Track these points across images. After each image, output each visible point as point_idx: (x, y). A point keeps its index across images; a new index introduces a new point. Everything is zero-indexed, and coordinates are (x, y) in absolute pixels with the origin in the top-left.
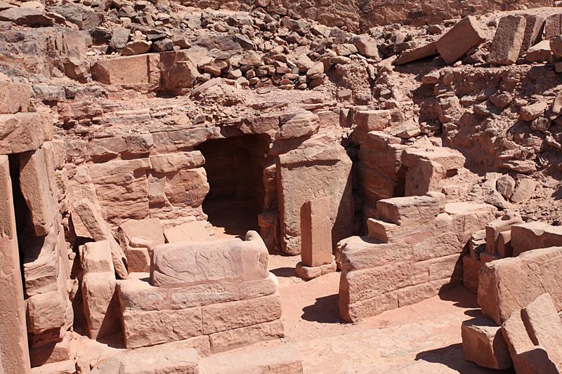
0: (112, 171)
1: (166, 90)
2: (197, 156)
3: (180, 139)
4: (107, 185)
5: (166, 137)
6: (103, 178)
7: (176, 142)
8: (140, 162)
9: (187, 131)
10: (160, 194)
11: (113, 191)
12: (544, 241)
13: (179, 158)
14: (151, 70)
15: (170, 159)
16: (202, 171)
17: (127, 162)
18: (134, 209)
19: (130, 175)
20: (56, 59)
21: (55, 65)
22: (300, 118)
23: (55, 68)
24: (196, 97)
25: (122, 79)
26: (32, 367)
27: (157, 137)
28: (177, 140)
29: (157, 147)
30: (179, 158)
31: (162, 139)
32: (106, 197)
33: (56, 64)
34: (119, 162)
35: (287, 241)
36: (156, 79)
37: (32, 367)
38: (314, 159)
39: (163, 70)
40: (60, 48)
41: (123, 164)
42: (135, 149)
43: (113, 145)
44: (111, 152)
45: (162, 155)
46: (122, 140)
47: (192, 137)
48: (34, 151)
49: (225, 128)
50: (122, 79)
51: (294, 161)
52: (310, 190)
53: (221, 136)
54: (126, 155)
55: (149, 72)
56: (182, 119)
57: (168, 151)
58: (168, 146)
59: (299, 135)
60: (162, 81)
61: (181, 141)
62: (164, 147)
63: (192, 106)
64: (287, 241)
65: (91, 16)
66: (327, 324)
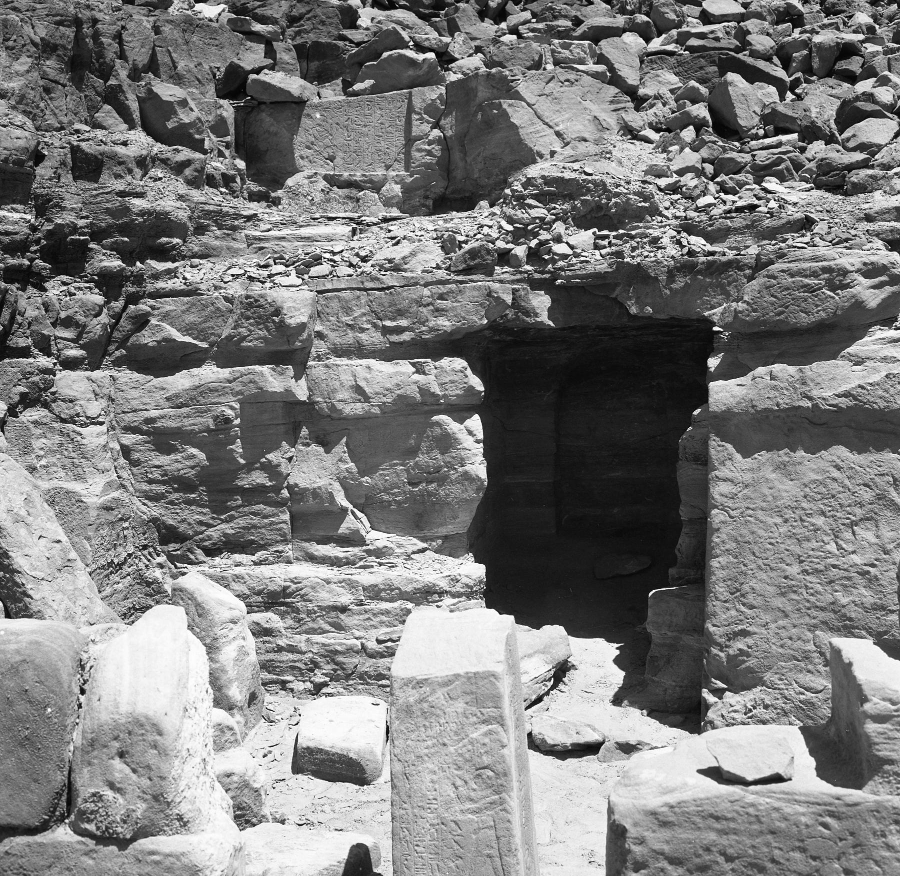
0: (177, 396)
1: (444, 191)
2: (456, 374)
3: (401, 313)
4: (164, 440)
5: (359, 306)
6: (153, 413)
7: (388, 323)
8: (262, 374)
9: (426, 292)
10: (321, 483)
11: (179, 456)
12: (128, 77)
14: (415, 132)
15: (361, 373)
16: (469, 434)
17: (226, 373)
18: (241, 522)
19: (230, 413)
20: (112, 82)
21: (106, 101)
22: (815, 259)
23: (107, 107)
25: (332, 159)
27: (335, 304)
28: (393, 319)
29: (331, 335)
31: (348, 310)
32: (156, 475)
33: (113, 97)
34: (210, 373)
35: (710, 698)
38: (844, 402)
39: (449, 133)
40: (139, 55)
41: (213, 378)
42: (256, 337)
43: (191, 318)
44: (188, 339)
45: (344, 361)
46: (223, 305)
47: (439, 312)
49: (571, 293)
50: (332, 159)
51: (761, 406)
52: (820, 521)
53: (544, 318)
54: (230, 354)
55: (410, 141)
56: (421, 256)
57: (360, 351)
58: (364, 337)
59: (804, 319)
60: (445, 165)
61: (404, 323)
64: (710, 698)
65: (319, 11)
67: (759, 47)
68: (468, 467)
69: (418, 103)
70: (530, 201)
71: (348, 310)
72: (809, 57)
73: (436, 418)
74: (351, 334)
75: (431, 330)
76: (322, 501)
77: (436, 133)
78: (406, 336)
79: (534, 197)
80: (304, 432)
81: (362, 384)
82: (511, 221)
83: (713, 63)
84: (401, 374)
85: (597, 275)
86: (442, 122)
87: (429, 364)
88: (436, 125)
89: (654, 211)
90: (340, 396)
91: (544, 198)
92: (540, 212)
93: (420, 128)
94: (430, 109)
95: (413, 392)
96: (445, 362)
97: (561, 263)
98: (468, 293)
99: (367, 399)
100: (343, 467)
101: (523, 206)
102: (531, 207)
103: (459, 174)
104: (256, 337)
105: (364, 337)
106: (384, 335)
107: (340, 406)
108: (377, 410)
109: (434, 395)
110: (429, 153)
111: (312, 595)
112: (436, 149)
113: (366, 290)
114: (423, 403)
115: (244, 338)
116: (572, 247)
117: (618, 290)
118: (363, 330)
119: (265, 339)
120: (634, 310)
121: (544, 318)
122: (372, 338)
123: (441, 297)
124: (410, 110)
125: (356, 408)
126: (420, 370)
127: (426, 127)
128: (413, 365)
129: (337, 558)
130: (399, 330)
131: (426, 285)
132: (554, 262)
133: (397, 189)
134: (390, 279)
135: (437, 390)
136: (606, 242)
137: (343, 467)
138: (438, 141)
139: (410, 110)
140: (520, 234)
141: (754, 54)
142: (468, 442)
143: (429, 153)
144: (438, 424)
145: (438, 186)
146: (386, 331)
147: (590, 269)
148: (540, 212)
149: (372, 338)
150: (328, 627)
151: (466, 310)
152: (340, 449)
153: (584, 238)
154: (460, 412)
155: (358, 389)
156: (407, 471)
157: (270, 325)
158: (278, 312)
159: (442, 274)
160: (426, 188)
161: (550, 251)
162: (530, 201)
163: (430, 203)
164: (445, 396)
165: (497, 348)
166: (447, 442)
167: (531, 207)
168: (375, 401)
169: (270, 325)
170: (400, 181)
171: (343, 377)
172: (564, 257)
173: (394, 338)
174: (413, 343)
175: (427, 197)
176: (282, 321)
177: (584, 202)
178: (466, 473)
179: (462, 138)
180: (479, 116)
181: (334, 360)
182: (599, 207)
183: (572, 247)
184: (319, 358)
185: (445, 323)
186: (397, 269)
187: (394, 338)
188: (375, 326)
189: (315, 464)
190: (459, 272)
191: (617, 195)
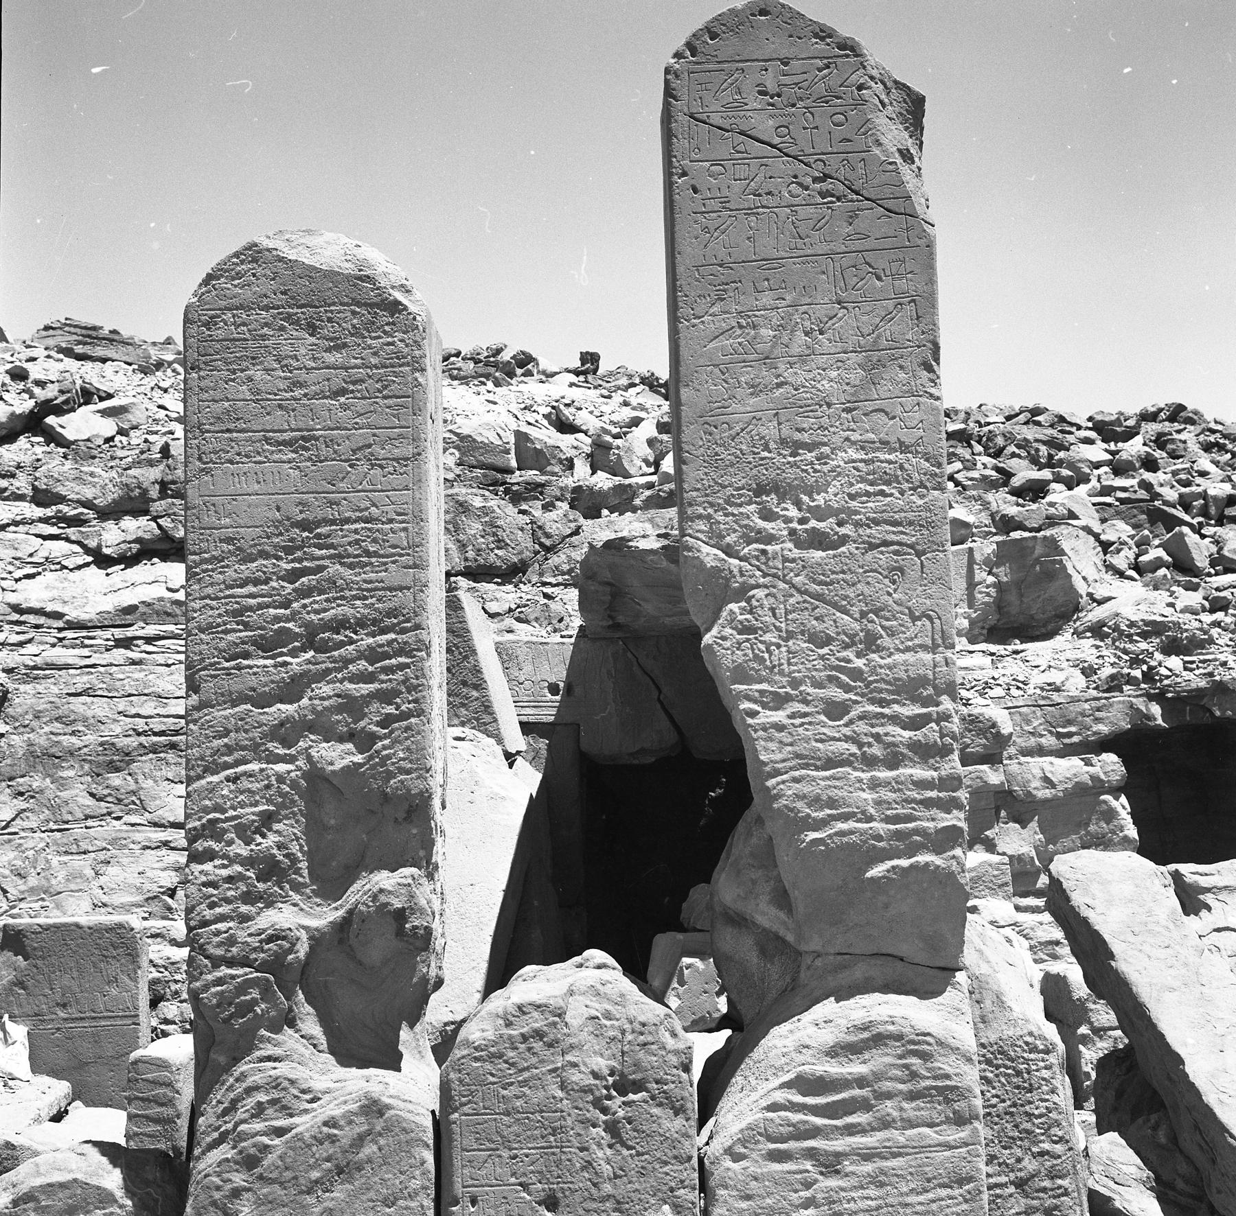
2: (1110, 765)
3: (1070, 722)
9: (1087, 706)
13: (1068, 769)
14: (977, 578)
15: (1048, 768)
24: (1097, 630)
26: (399, 1070)
28: (1064, 727)
30: (1068, 769)
31: (1028, 722)
36: (987, 599)
37: (399, 1070)
45: (1028, 759)
48: (9, 604)
49: (1174, 702)
53: (1160, 721)
55: (971, 585)
56: (1071, 680)
57: (1041, 751)
58: (1043, 740)
60: (999, 605)
61: (1073, 729)
62: (1033, 741)
63: (1087, 649)
66: (372, 1071)
67: (1168, 498)
68: (1126, 832)
69: (978, 557)
70: (1135, 638)
71: (1028, 722)
72: (1206, 506)
73: (1102, 797)
74: (1033, 739)
75: (1095, 733)
76: (1025, 864)
77: (991, 579)
78: (1076, 739)
79: (1138, 634)
80: (1003, 813)
81: (1049, 775)
82: (1126, 652)
83: (1143, 512)
84: (1076, 767)
85: (1199, 690)
86: (995, 570)
87: (1095, 759)
88: (990, 573)
89: (1211, 641)
90: (1033, 785)
91: (1145, 635)
92: (1143, 645)
93: (980, 575)
94: (987, 561)
95: (1086, 779)
96: (1104, 756)
97: (1166, 682)
98: (1116, 706)
99: (1053, 786)
100: (1037, 837)
101: (1132, 641)
102: (1137, 642)
103: (1014, 610)
104: (978, 745)
105: (1043, 740)
106: (1058, 739)
107: (1035, 792)
108: (1061, 794)
109: (1102, 781)
110: (988, 594)
111: (1032, 934)
112: (992, 591)
113: (1039, 706)
114: (1093, 787)
115: (968, 746)
116: (1170, 670)
117: (1205, 700)
118: (1042, 736)
119: (984, 745)
120: (1218, 713)
121: (1160, 721)
122: (1049, 741)
123: (1098, 710)
124: (971, 561)
125: (1047, 793)
126: (1088, 763)
127: (984, 574)
128: (1082, 759)
129: (1037, 907)
130: (1070, 735)
131: (1086, 701)
132: (1161, 681)
133: (966, 623)
134: (1056, 697)
135: (1103, 777)
136: (1194, 666)
137: (1037, 837)
138: (994, 585)
139: (971, 561)
140: (1135, 661)
141: (1166, 503)
142: (1120, 809)
143: (988, 594)
144: (1105, 802)
145: (992, 619)
146: (1059, 736)
147: (1194, 686)
148: (1143, 645)
149: (1049, 741)
150: (1047, 958)
151: (1114, 719)
152: (1034, 825)
153: (1175, 662)
154: (1116, 791)
155: (1046, 779)
156: (1081, 838)
157: (989, 735)
158: (994, 725)
159: (1094, 693)
160: (984, 620)
161: (1157, 673)
162: (1135, 638)
163: (985, 632)
164: (1109, 781)
165: (1131, 744)
166: (1110, 815)
167: (1137, 642)
168: (1060, 788)
169: (989, 735)
170: (968, 617)
171: (1034, 771)
172: (1168, 677)
173: (1067, 741)
174: (1080, 743)
175: (983, 628)
176: (999, 732)
177: (1167, 637)
178: (1126, 836)
179: (1018, 584)
180: (1038, 568)
181: (1023, 759)
182: (1175, 639)
183: (1170, 670)
184: (1010, 758)
185: (1104, 729)
186: (1058, 690)
187: (1067, 741)
188: (1050, 732)
189: (1015, 837)
190: (1104, 691)
191: (1186, 630)
